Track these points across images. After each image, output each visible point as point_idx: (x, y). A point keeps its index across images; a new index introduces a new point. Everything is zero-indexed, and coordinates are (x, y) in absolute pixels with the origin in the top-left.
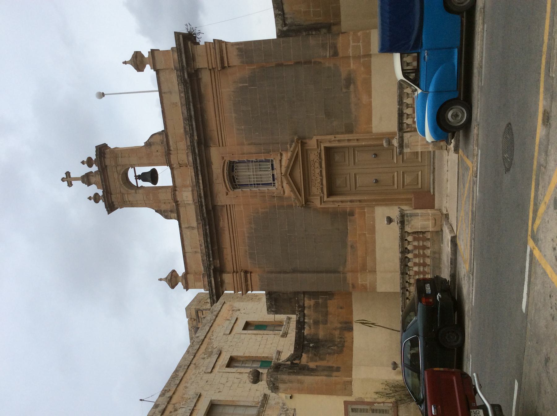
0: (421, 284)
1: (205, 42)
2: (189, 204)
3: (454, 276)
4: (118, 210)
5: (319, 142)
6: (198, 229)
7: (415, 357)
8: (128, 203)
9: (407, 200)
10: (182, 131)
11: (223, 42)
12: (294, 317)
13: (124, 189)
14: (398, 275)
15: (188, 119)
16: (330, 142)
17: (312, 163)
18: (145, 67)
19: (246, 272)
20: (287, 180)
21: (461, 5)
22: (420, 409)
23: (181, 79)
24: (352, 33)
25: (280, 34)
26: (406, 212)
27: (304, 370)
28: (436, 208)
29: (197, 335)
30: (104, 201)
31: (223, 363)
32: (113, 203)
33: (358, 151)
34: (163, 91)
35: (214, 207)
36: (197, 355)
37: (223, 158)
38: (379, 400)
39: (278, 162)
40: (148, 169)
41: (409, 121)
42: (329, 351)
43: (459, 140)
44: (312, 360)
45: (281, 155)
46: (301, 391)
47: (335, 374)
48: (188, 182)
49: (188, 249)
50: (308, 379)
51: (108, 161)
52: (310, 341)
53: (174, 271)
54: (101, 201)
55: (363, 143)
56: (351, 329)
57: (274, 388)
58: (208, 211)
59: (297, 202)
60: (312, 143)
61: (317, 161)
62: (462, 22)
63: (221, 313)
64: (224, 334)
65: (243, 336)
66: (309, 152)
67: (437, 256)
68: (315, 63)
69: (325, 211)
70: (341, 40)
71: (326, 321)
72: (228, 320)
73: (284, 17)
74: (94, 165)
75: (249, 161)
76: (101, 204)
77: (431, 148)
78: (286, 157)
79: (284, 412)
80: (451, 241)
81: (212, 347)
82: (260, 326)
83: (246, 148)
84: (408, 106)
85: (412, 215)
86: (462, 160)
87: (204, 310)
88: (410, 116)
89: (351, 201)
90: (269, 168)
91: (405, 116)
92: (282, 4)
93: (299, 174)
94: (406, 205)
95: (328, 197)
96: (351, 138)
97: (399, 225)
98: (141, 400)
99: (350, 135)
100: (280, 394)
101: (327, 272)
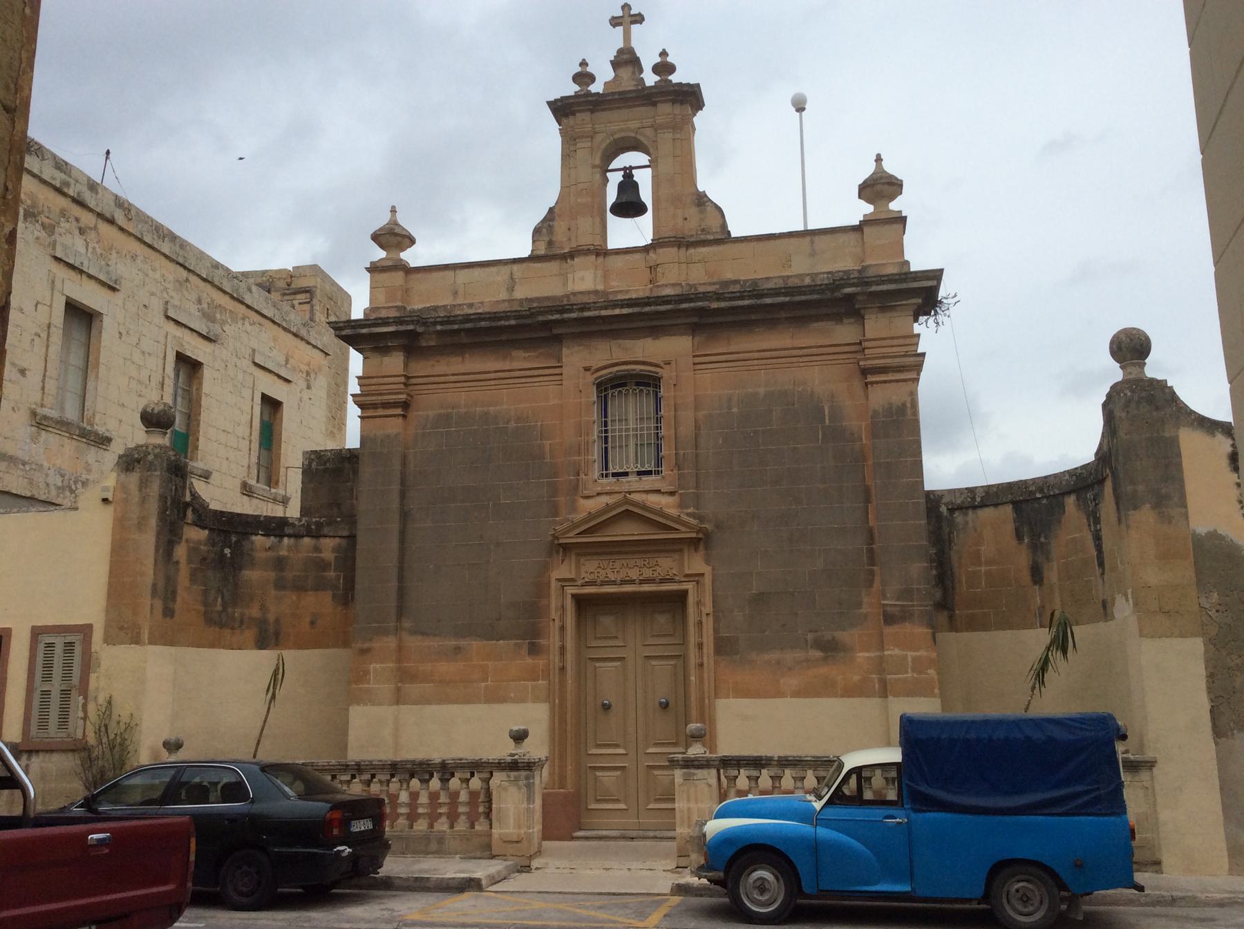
0: (373, 808)
1: (918, 335)
2: (565, 284)
3: (388, 885)
4: (556, 126)
5: (697, 578)
6: (509, 301)
7: (201, 793)
8: (572, 148)
9: (563, 778)
10: (729, 276)
11: (919, 374)
12: (293, 511)
13: (602, 141)
14: (387, 755)
15: (754, 290)
16: (698, 603)
17: (652, 562)
18: (869, 201)
19: (406, 405)
20: (616, 505)
21: (1005, 901)
22: (72, 804)
23: (842, 279)
24: (934, 655)
25: (934, 499)
26: (537, 773)
27: (171, 531)
28: (545, 843)
29: (254, 288)
30: (577, 95)
31: (187, 346)
32: (573, 113)
33: (675, 666)
34: (817, 238)
35: (558, 339)
36: (209, 286)
37: (668, 363)
38: (91, 707)
39: (657, 486)
40: (646, 195)
41: (742, 782)
42: (213, 593)
43: (701, 896)
44: (193, 550)
45: (672, 494)
46: (120, 524)
47: (159, 604)
48: (615, 284)
49: (463, 276)
50: (147, 541)
51: (665, 110)
52: (236, 549)
53: (412, 241)
54: (577, 88)
55: (693, 678)
56: (261, 644)
57: (129, 462)
58: (547, 325)
59: (565, 525)
60: (696, 563)
61: (656, 574)
62: (969, 900)
63: (302, 345)
64: (254, 351)
65: (247, 393)
66: (676, 556)
67: (434, 846)
68: (872, 573)
69: (541, 589)
70: (922, 631)
71: (283, 588)
72: (287, 361)
73: (967, 508)
74: (657, 78)
75: (658, 420)
76: (571, 89)
77: (682, 831)
78: (666, 504)
79: (66, 483)
80: (471, 880)
81: (224, 322)
82: (269, 435)
83: (687, 417)
84: (776, 778)
85: (530, 787)
86: (659, 903)
87: (312, 307)
88: (753, 784)
89: (563, 649)
90: (643, 465)
91: (754, 773)
92: (996, 505)
93: (629, 531)
94: (551, 774)
95: (573, 595)
96: (705, 650)
97: (509, 759)
98: (108, 153)
99: (712, 651)
100: (114, 475)
101: (401, 593)
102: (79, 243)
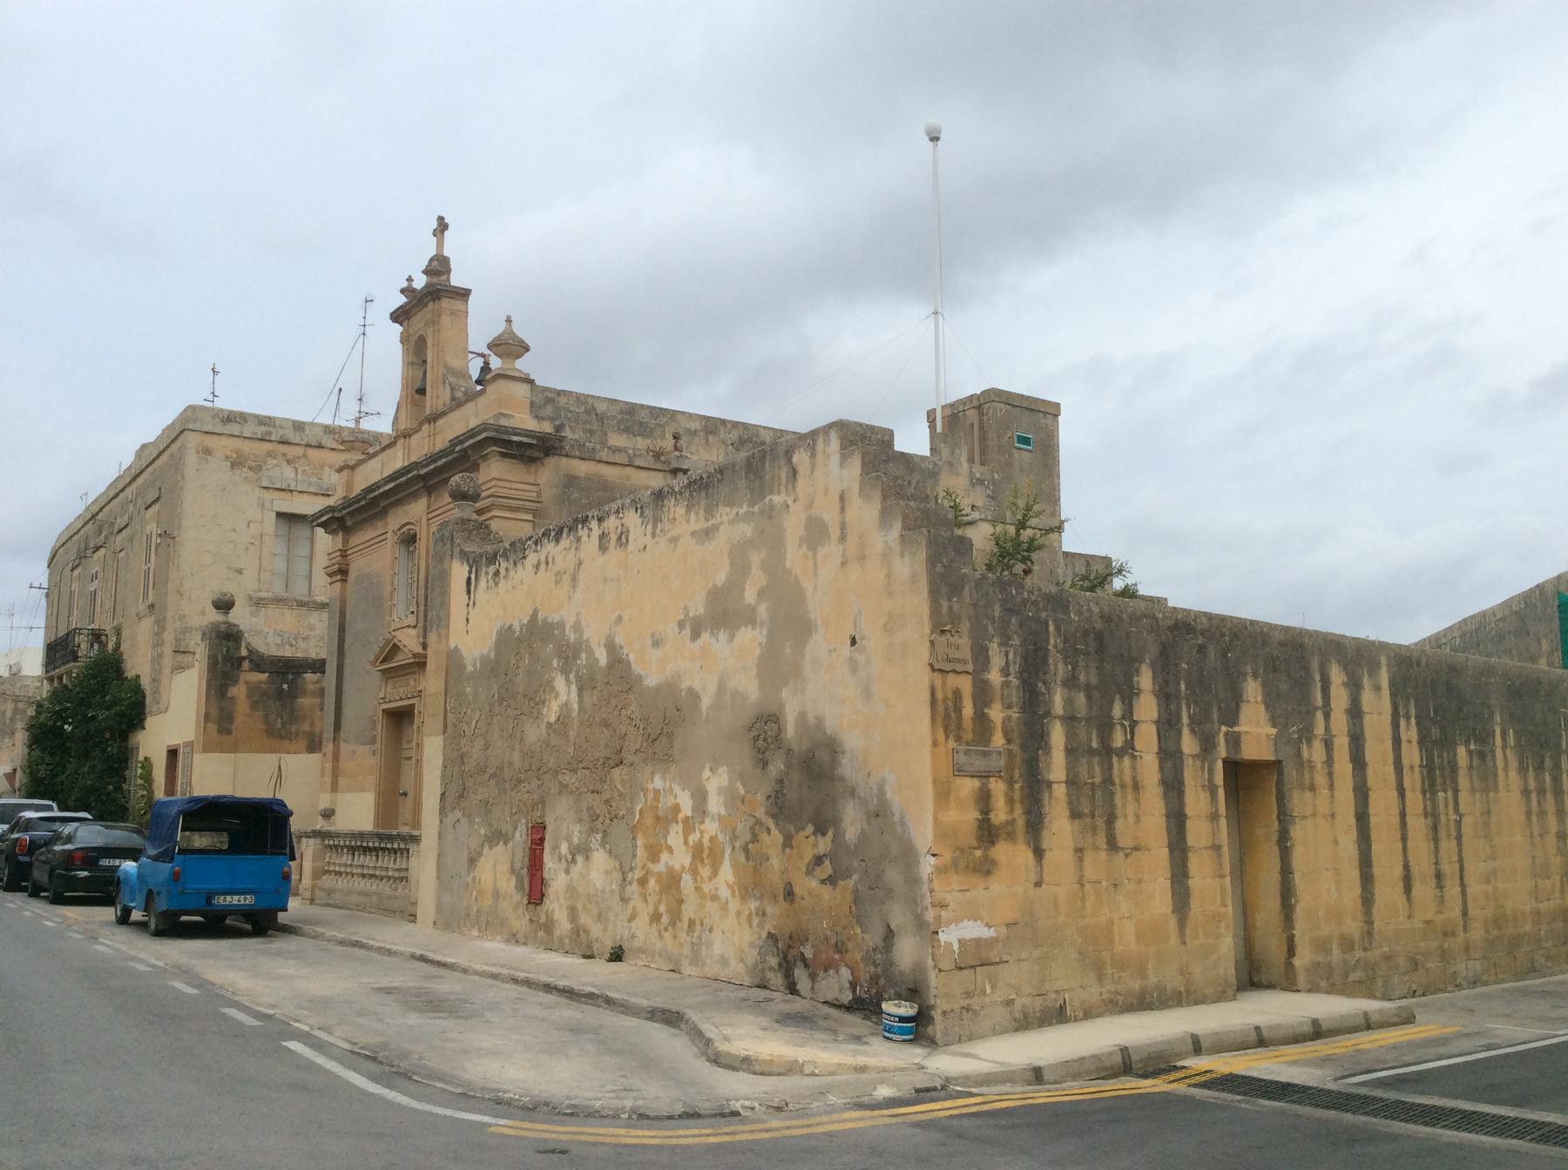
44: (253, 689)
102: (288, 472)
